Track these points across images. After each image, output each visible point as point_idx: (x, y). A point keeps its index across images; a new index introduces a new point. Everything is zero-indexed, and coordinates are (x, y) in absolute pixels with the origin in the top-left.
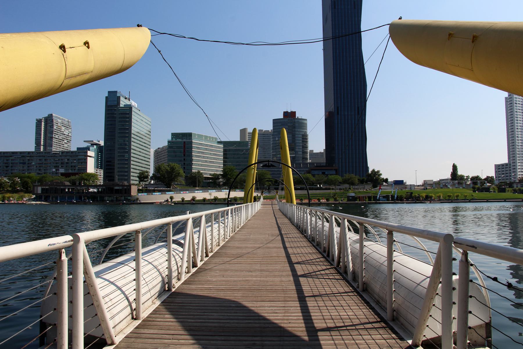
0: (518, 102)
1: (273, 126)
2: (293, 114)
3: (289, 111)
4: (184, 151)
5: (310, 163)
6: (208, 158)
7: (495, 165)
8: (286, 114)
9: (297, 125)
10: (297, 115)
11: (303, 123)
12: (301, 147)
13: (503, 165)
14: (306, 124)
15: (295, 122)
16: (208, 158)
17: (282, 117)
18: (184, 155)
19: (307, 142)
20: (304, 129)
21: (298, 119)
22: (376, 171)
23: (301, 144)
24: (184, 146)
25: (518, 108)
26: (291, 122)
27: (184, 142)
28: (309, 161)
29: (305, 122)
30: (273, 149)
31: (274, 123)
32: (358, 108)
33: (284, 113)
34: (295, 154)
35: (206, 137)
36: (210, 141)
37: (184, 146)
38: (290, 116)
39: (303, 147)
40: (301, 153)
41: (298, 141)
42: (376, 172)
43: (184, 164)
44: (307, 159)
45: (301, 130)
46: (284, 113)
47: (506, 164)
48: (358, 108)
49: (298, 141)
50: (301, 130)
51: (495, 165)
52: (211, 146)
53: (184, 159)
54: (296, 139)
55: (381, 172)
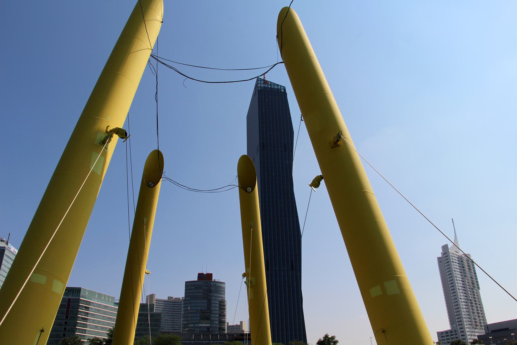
0: (454, 261)
1: (185, 293)
2: (210, 276)
3: (205, 273)
4: (68, 311)
5: (227, 334)
6: (99, 322)
7: (438, 333)
8: (201, 276)
9: (213, 288)
10: (214, 278)
11: (221, 287)
12: (218, 315)
13: (446, 332)
14: (224, 288)
15: (210, 285)
16: (99, 322)
17: (196, 279)
18: (67, 317)
19: (225, 309)
20: (220, 294)
21: (215, 282)
22: (322, 339)
23: (218, 312)
24: (69, 305)
25: (456, 267)
26: (205, 290)
27: (69, 299)
28: (226, 332)
29: (223, 285)
30: (184, 317)
31: (186, 286)
32: (292, 262)
33: (199, 274)
34: (211, 324)
35: (100, 295)
36: (104, 300)
37: (69, 305)
38: (205, 278)
39: (220, 315)
40: (218, 322)
41: (214, 308)
42: (330, 338)
43: (65, 329)
44: (224, 330)
45: (218, 295)
46: (199, 274)
47: (451, 331)
48: (292, 262)
49: (214, 308)
50: (218, 295)
51: (438, 333)
52: (106, 307)
53: (66, 323)
54: (212, 305)
55: (336, 339)
